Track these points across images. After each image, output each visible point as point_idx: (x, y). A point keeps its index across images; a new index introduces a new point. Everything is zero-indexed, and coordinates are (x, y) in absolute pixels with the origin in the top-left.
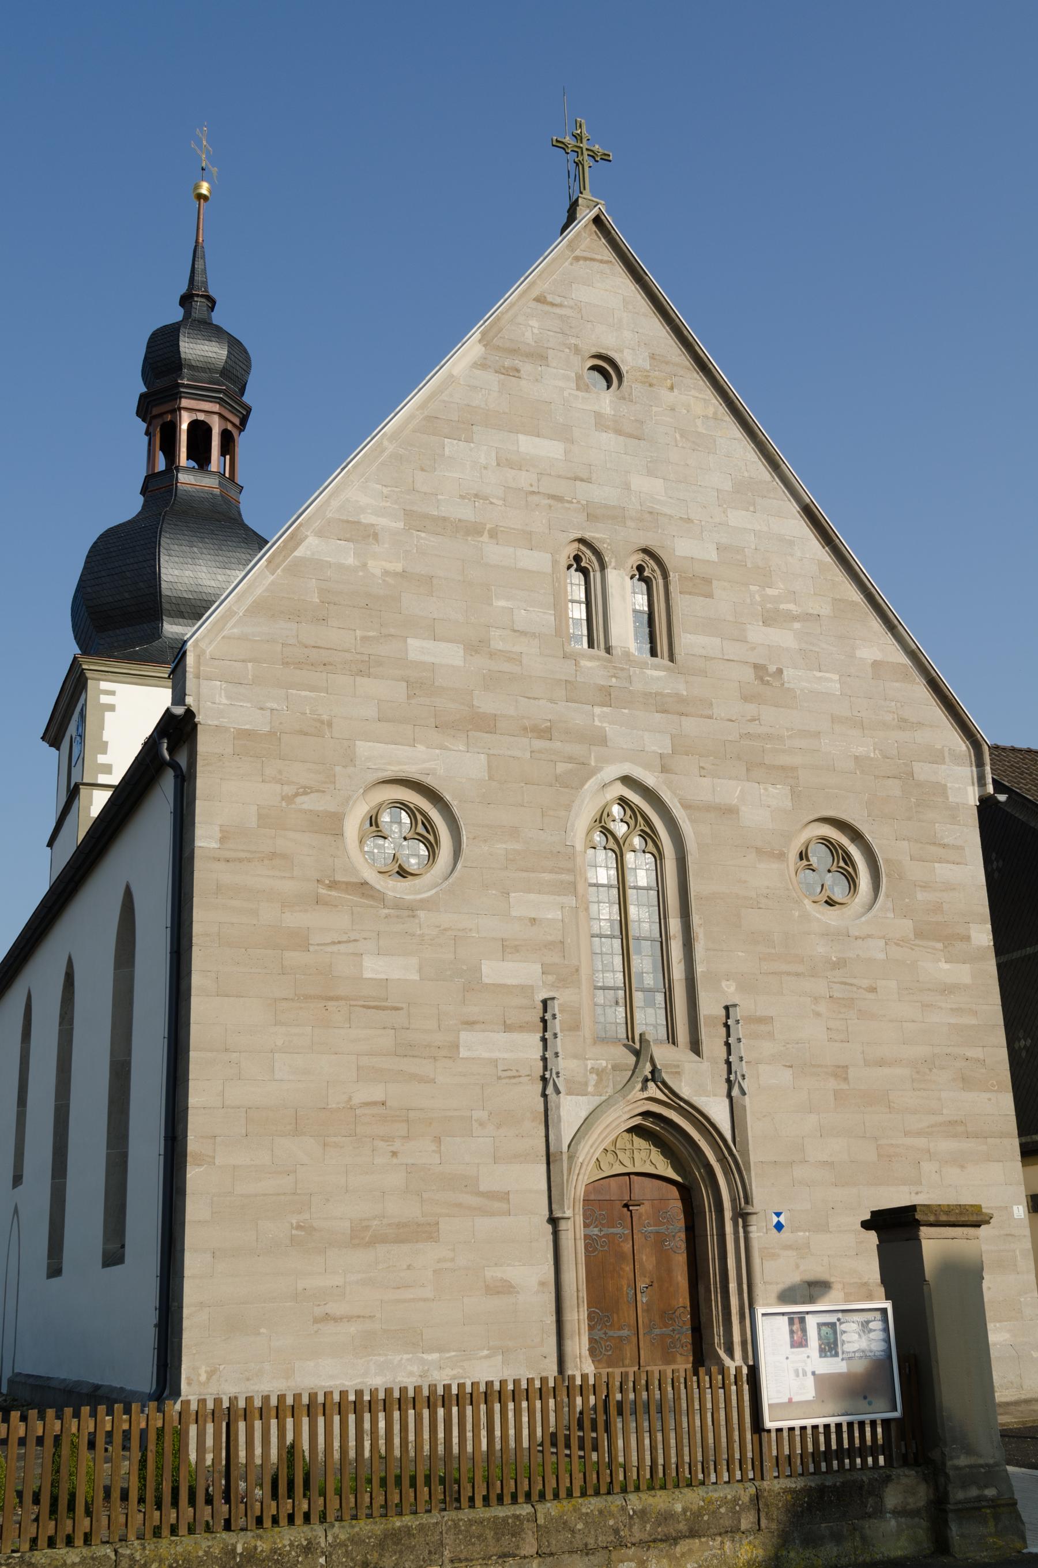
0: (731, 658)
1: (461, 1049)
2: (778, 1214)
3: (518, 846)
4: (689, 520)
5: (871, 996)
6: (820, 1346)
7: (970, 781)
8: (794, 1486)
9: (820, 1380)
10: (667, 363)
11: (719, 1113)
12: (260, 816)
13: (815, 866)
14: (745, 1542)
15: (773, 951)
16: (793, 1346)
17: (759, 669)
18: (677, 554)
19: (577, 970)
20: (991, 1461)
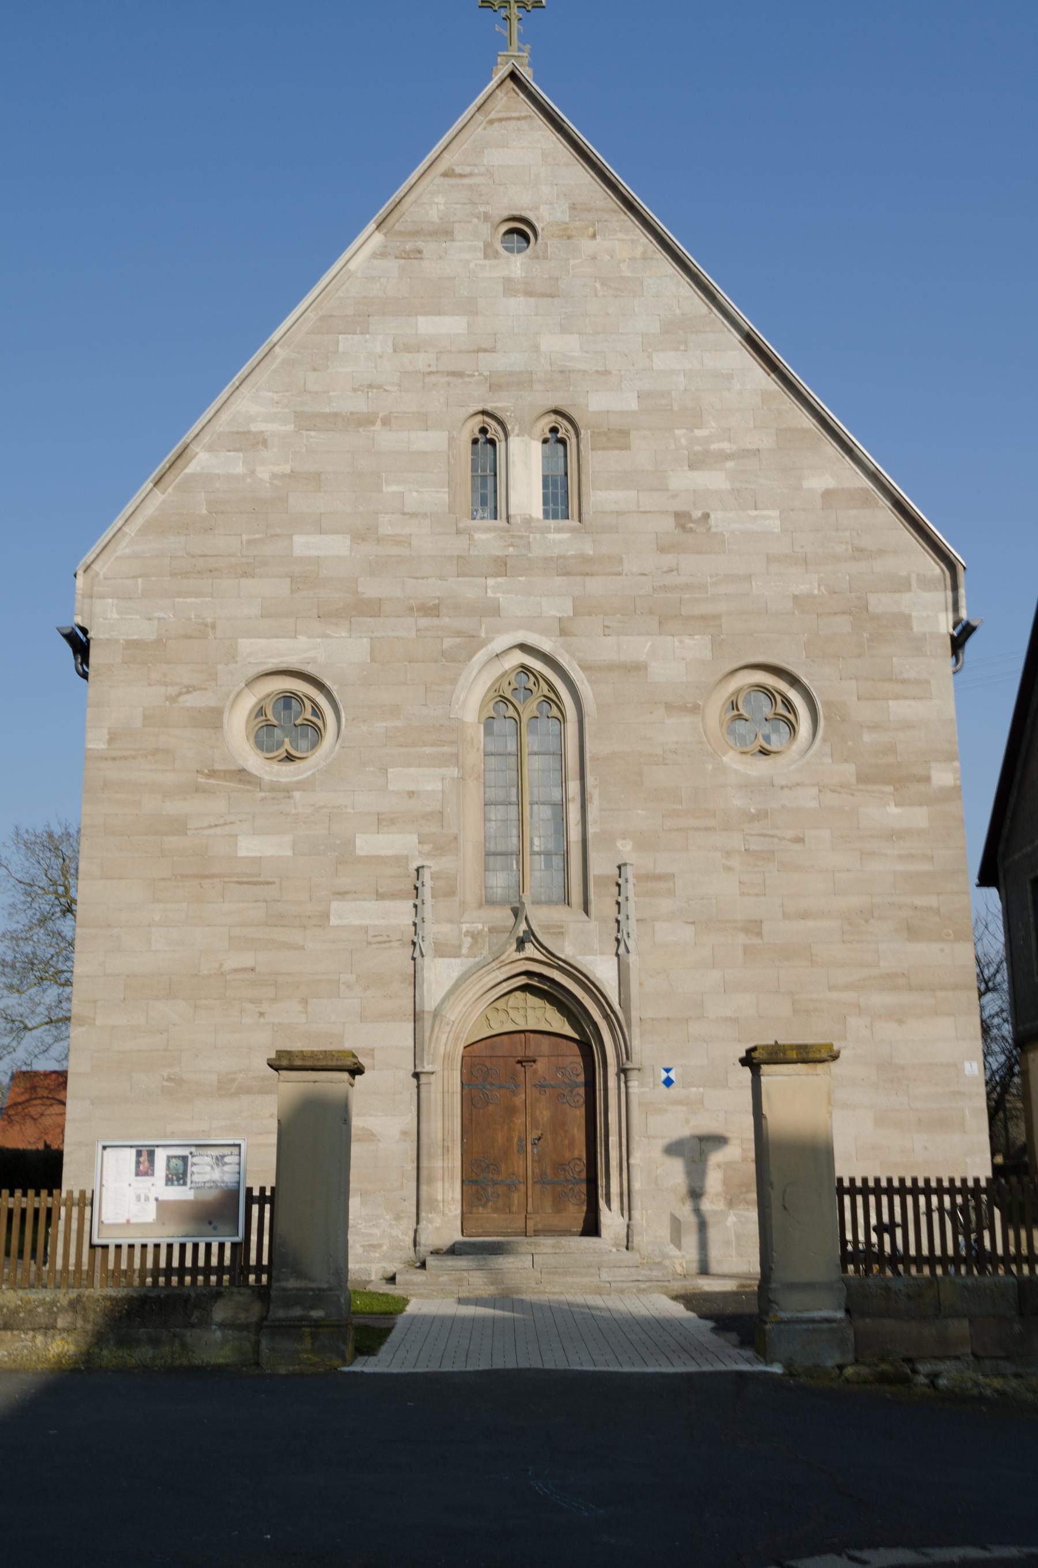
0: (648, 509)
1: (332, 918)
2: (668, 1070)
3: (398, 724)
4: (607, 372)
5: (798, 847)
6: (167, 1176)
7: (944, 608)
8: (114, 1294)
9: (162, 1206)
10: (589, 211)
11: (604, 971)
12: (145, 717)
13: (746, 715)
14: (58, 1338)
15: (679, 807)
16: (137, 1174)
17: (681, 518)
18: (590, 409)
19: (456, 838)
20: (325, 1286)
